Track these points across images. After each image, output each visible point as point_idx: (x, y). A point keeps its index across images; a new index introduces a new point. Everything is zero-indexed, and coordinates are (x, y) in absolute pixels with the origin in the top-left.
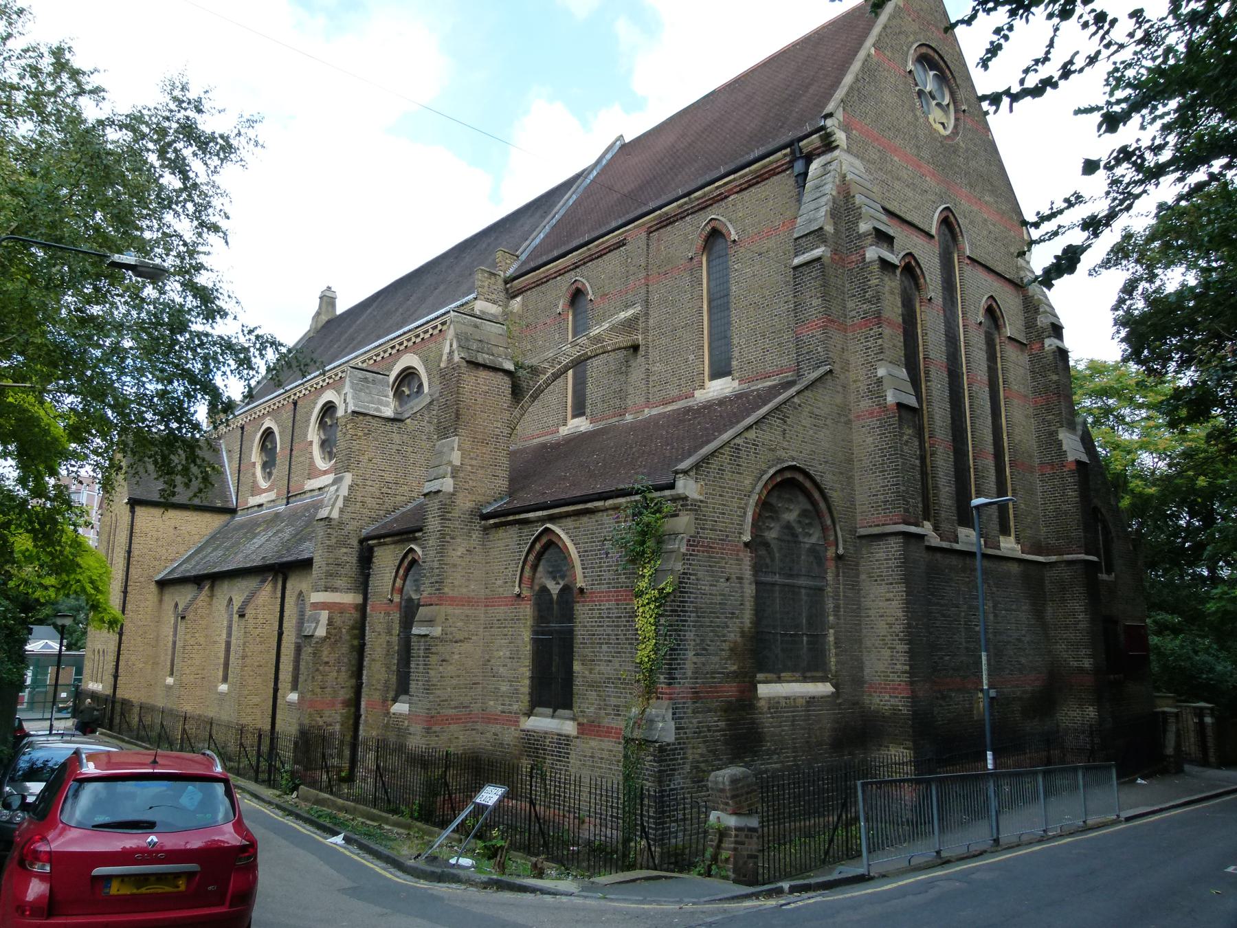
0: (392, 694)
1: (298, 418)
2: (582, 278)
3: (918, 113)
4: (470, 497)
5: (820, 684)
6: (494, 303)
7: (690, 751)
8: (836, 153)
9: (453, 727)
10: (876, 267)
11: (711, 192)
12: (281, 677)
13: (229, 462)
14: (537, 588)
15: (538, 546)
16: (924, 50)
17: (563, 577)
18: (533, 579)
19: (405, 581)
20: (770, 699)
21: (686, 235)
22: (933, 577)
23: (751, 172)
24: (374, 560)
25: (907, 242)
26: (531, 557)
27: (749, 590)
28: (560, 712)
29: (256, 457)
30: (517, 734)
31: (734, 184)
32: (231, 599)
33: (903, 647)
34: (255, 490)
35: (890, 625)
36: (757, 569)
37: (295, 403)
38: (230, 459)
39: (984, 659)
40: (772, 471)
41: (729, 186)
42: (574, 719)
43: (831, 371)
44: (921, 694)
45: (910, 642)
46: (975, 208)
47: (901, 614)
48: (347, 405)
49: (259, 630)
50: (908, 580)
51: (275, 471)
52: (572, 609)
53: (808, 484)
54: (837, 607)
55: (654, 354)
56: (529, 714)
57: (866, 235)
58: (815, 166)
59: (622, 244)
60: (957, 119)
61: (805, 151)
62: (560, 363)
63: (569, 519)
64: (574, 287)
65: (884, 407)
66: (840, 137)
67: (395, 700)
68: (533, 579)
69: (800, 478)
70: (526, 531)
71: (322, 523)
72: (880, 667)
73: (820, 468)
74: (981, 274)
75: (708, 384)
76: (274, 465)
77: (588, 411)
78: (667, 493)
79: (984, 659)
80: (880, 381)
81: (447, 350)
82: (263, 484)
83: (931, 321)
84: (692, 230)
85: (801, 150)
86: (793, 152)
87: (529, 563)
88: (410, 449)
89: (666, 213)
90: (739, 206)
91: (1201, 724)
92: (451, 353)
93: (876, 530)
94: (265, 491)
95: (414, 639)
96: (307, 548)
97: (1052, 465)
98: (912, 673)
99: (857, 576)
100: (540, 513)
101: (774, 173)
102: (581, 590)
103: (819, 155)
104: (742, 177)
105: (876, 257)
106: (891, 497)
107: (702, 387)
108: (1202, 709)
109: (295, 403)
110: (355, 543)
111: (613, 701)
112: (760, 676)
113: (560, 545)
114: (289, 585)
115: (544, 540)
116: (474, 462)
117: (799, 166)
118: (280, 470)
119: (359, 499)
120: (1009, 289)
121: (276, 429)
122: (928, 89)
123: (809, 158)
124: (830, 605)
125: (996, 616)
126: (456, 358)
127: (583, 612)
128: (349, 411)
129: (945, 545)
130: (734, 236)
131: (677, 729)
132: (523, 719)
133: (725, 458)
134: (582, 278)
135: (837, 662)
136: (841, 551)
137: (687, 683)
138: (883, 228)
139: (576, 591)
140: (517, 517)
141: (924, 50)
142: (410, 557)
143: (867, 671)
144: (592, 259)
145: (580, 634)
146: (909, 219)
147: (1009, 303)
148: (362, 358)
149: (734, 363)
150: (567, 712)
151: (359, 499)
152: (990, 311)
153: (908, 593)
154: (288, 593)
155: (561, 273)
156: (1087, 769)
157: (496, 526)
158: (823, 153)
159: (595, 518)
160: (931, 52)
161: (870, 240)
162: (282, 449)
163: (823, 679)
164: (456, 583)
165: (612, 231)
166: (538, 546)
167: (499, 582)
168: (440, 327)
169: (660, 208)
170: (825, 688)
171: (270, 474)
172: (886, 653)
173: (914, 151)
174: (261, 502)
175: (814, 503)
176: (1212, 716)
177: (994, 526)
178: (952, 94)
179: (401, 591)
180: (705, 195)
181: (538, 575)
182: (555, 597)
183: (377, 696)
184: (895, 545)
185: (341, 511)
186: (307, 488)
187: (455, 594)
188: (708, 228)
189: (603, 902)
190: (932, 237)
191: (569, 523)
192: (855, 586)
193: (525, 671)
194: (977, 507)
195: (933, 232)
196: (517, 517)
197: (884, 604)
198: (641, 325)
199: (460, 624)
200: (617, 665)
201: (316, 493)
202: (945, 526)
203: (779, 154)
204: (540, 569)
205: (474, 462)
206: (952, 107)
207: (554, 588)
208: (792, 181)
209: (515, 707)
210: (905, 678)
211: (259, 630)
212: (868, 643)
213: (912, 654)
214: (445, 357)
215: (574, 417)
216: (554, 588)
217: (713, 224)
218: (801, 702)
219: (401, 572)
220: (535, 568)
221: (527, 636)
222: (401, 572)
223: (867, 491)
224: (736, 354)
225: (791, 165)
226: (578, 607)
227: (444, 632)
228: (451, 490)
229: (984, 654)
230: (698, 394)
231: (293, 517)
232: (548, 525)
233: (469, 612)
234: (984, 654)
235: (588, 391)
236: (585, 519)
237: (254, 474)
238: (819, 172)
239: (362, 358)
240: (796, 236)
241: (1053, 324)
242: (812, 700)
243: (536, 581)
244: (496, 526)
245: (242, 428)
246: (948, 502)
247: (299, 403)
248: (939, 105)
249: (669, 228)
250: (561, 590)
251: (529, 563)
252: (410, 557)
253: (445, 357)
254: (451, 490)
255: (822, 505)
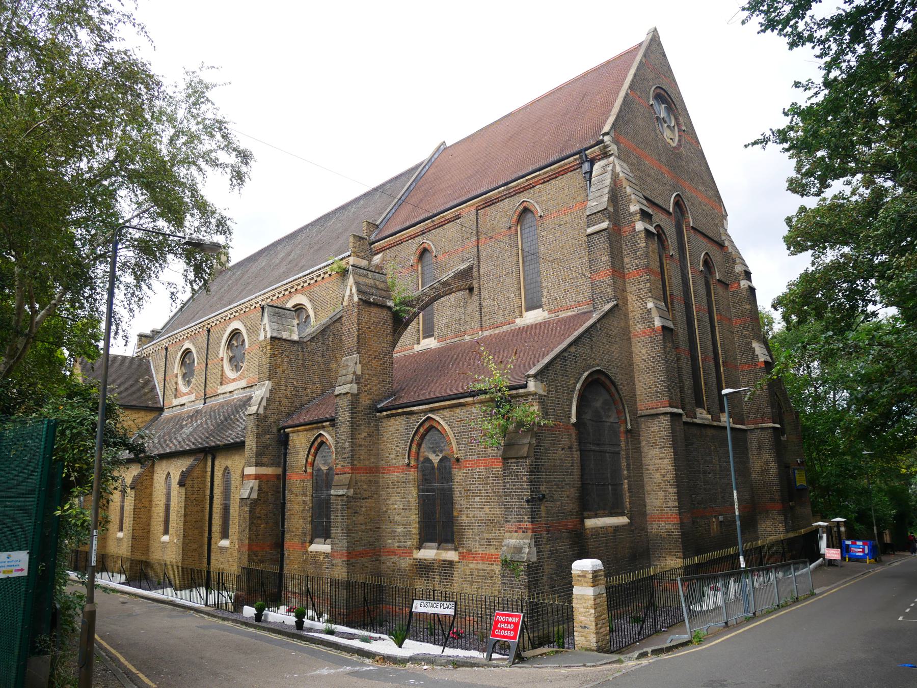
0: (308, 539)
1: (211, 341)
2: (428, 241)
3: (658, 132)
4: (369, 397)
5: (620, 518)
6: (363, 258)
7: (546, 567)
8: (611, 159)
9: (364, 559)
10: (643, 235)
11: (523, 183)
12: (214, 529)
13: (157, 374)
14: (421, 459)
15: (422, 430)
16: (659, 91)
17: (441, 451)
18: (418, 453)
19: (315, 457)
20: (592, 529)
21: (505, 212)
22: (689, 440)
23: (551, 170)
24: (290, 443)
25: (660, 218)
26: (417, 438)
27: (576, 455)
28: (443, 545)
29: (177, 369)
30: (411, 562)
31: (539, 178)
32: (169, 474)
33: (673, 490)
34: (176, 394)
35: (664, 476)
36: (580, 441)
37: (209, 331)
38: (157, 371)
39: (735, 494)
40: (586, 374)
41: (536, 179)
42: (456, 550)
43: (617, 305)
44: (685, 521)
45: (678, 487)
46: (694, 195)
47: (670, 468)
48: (266, 332)
49: (195, 496)
50: (674, 445)
51: (193, 380)
52: (450, 473)
53: (608, 382)
54: (628, 464)
55: (484, 294)
56: (419, 548)
57: (635, 213)
58: (597, 166)
59: (458, 217)
60: (680, 136)
61: (589, 157)
62: (423, 301)
63: (445, 411)
64: (422, 247)
65: (653, 329)
66: (613, 148)
67: (311, 543)
68: (418, 453)
69: (603, 378)
70: (413, 418)
71: (252, 417)
72: (658, 503)
73: (614, 371)
74: (700, 239)
75: (525, 314)
76: (193, 375)
77: (436, 334)
78: (521, 391)
79: (735, 494)
80: (649, 311)
81: (348, 293)
82: (183, 389)
83: (672, 269)
84: (511, 206)
85: (586, 156)
86: (581, 158)
87: (415, 442)
88: (310, 363)
89: (490, 197)
90: (543, 192)
91: (839, 531)
92: (351, 295)
93: (653, 412)
94: (186, 394)
95: (333, 498)
96: (230, 435)
97: (749, 364)
98: (680, 507)
99: (640, 443)
100: (423, 407)
101: (565, 172)
102: (458, 460)
103: (599, 160)
104: (545, 173)
105: (642, 228)
106: (660, 389)
107: (521, 316)
108: (838, 522)
109: (209, 331)
110: (275, 430)
111: (486, 536)
112: (586, 514)
113: (439, 428)
114: (217, 463)
115: (427, 425)
116: (370, 372)
117: (586, 166)
118: (197, 379)
119: (277, 399)
120: (715, 248)
121: (193, 349)
122: (662, 116)
123: (592, 162)
124: (624, 463)
125: (720, 466)
126: (356, 299)
127: (458, 474)
128: (269, 336)
129: (689, 420)
130: (540, 213)
131: (538, 552)
132: (415, 552)
133: (558, 366)
134: (428, 241)
135: (630, 502)
136: (629, 427)
137: (543, 520)
138: (645, 209)
139: (453, 460)
140: (405, 410)
141: (659, 91)
142: (319, 440)
143: (648, 507)
144: (435, 227)
145: (457, 489)
146: (657, 202)
147: (717, 257)
148: (261, 298)
149: (544, 300)
150: (450, 546)
151: (277, 399)
152: (706, 263)
153: (675, 453)
154: (216, 468)
155: (412, 237)
156: (795, 564)
157: (388, 416)
158: (602, 159)
159: (465, 409)
160: (662, 92)
161: (638, 217)
162: (199, 364)
163: (622, 514)
164: (362, 458)
165: (451, 209)
166: (422, 430)
167: (392, 456)
168: (322, 276)
169: (486, 193)
170: (623, 520)
171: (189, 382)
172: (662, 494)
173: (657, 157)
174: (183, 402)
175: (611, 395)
176: (845, 526)
177: (716, 407)
178: (676, 119)
179: (312, 464)
180: (518, 185)
181: (422, 450)
182: (436, 465)
183: (296, 540)
184: (665, 421)
185: (265, 408)
186: (219, 391)
187: (362, 465)
188: (521, 207)
189: (583, 669)
190: (670, 214)
191: (446, 413)
192: (638, 450)
193: (414, 517)
194: (726, 395)
195: (671, 210)
196: (405, 410)
197: (659, 461)
198: (476, 274)
199: (365, 486)
200: (488, 511)
201: (228, 395)
202: (688, 407)
203: (571, 159)
204: (423, 445)
205: (370, 372)
206: (676, 128)
207: (435, 459)
208: (581, 176)
209: (409, 543)
210: (676, 510)
211: (195, 496)
212: (648, 488)
213: (679, 494)
214: (346, 298)
215: (424, 338)
216: (435, 459)
217: (524, 204)
218: (610, 530)
219: (313, 450)
220: (419, 445)
221: (414, 492)
222: (313, 450)
223: (648, 383)
224: (545, 293)
225: (580, 166)
226: (455, 471)
227: (355, 493)
228: (356, 392)
229: (735, 492)
230: (518, 321)
231: (212, 413)
232: (430, 415)
233: (371, 478)
234: (735, 492)
235: (435, 320)
236: (458, 410)
237: (176, 382)
238: (599, 172)
239: (261, 298)
240: (588, 213)
241: (745, 271)
242: (617, 528)
243: (421, 454)
244: (388, 416)
245: (166, 349)
246: (689, 391)
247: (212, 330)
248: (669, 126)
249: (492, 207)
250: (441, 460)
251: (415, 442)
252: (319, 440)
253: (346, 298)
254: (356, 392)
255: (617, 396)
